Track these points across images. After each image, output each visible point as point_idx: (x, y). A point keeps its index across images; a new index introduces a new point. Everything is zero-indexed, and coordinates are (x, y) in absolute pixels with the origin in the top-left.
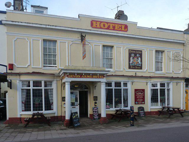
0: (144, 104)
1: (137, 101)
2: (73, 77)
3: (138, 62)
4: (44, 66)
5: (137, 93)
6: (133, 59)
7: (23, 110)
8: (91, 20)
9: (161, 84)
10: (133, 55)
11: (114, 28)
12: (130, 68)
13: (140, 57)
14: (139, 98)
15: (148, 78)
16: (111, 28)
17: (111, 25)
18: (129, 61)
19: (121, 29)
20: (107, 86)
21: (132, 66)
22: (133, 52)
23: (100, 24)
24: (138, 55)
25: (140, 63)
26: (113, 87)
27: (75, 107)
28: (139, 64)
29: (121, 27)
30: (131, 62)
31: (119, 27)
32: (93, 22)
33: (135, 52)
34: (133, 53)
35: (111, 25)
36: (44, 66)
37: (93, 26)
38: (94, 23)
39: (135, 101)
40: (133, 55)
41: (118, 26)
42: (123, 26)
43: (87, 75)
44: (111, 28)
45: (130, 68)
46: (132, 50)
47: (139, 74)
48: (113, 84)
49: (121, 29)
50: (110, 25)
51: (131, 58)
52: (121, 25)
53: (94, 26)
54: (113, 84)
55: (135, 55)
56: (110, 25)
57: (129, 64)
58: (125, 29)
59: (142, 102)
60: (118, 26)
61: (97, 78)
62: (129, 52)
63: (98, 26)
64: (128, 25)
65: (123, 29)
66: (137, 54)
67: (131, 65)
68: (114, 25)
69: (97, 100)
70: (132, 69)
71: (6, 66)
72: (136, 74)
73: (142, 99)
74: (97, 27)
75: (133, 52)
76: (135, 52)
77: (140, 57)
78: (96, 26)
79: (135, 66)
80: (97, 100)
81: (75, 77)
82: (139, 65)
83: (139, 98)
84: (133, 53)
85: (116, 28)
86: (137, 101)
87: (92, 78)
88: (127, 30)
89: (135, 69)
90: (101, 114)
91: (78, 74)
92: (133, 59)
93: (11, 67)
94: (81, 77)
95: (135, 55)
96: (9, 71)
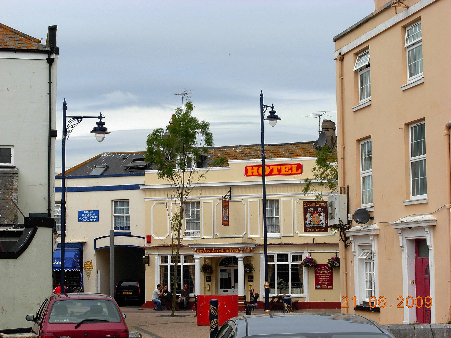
0: (332, 288)
1: (319, 284)
2: (203, 253)
3: (321, 221)
4: (417, 129)
5: (319, 270)
6: (310, 216)
7: (170, 314)
8: (245, 166)
9: (293, 256)
10: (311, 210)
11: (279, 172)
12: (305, 231)
13: (323, 211)
14: (322, 280)
15: (304, 247)
16: (275, 172)
17: (275, 169)
18: (305, 219)
19: (292, 171)
20: (164, 262)
21: (310, 227)
22: (311, 205)
23: (258, 169)
24: (319, 209)
25: (323, 221)
26: (275, 262)
27: (227, 291)
28: (323, 223)
29: (291, 169)
30: (307, 222)
31: (287, 169)
32: (248, 168)
33: (314, 205)
34: (311, 207)
35: (275, 169)
36: (417, 129)
37: (248, 174)
38: (250, 169)
39: (316, 284)
40: (311, 210)
41: (286, 168)
42: (294, 167)
43: (225, 250)
44: (275, 172)
45: (305, 231)
46: (308, 202)
47: (318, 241)
48: (290, 258)
49: (292, 171)
50: (273, 169)
51: (308, 215)
52: (291, 165)
53: (250, 173)
54: (290, 258)
55: (315, 209)
56: (273, 169)
57: (305, 224)
58: (297, 170)
59: (328, 285)
60: (286, 168)
61: (231, 252)
62: (304, 205)
63: (255, 173)
64: (302, 164)
65: (294, 171)
66: (318, 207)
67: (308, 226)
68: (279, 167)
69: (253, 281)
70: (310, 231)
71: (144, 238)
72: (314, 240)
73: (328, 280)
74: (254, 174)
75: (311, 205)
76: (314, 205)
77: (323, 211)
78: (253, 173)
79: (314, 227)
80: (253, 281)
81: (205, 253)
82: (322, 225)
83: (322, 280)
84: (311, 207)
85: (283, 172)
86: (319, 284)
87: (225, 252)
88: (301, 171)
89: (315, 231)
90: (201, 271)
91: (207, 249)
92: (310, 216)
93: (149, 239)
94: (211, 252)
95: (315, 209)
96: (147, 245)
